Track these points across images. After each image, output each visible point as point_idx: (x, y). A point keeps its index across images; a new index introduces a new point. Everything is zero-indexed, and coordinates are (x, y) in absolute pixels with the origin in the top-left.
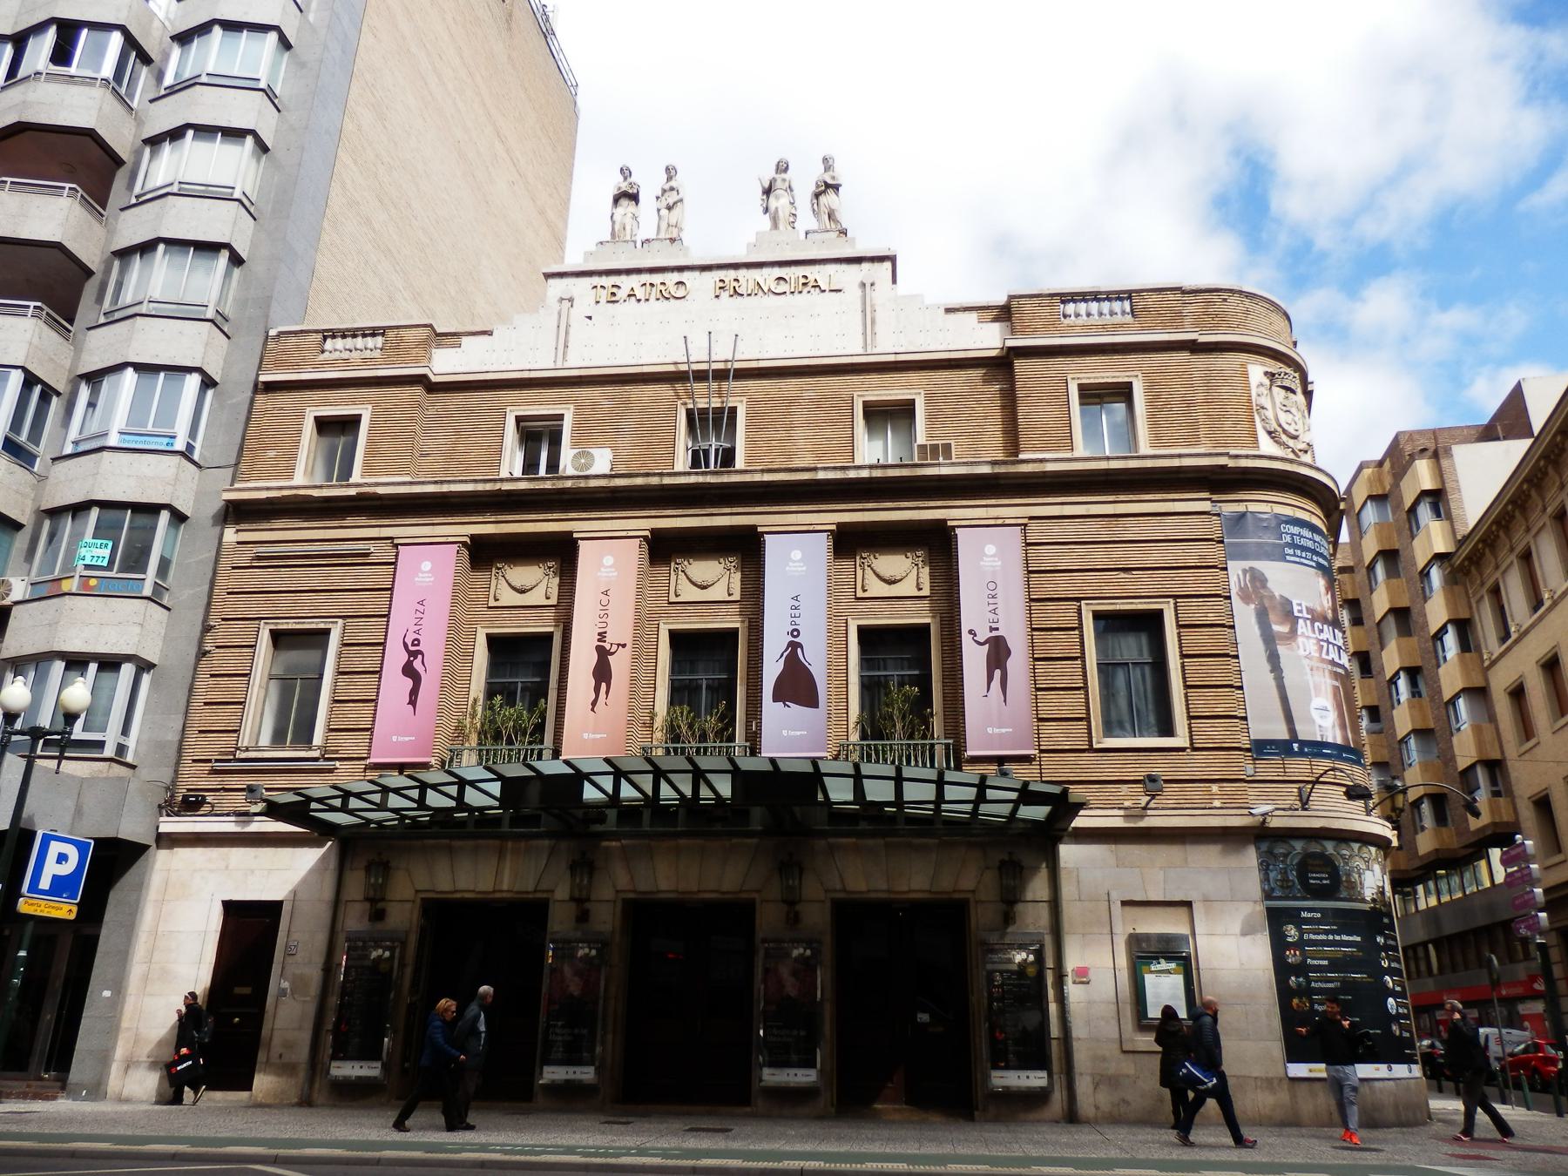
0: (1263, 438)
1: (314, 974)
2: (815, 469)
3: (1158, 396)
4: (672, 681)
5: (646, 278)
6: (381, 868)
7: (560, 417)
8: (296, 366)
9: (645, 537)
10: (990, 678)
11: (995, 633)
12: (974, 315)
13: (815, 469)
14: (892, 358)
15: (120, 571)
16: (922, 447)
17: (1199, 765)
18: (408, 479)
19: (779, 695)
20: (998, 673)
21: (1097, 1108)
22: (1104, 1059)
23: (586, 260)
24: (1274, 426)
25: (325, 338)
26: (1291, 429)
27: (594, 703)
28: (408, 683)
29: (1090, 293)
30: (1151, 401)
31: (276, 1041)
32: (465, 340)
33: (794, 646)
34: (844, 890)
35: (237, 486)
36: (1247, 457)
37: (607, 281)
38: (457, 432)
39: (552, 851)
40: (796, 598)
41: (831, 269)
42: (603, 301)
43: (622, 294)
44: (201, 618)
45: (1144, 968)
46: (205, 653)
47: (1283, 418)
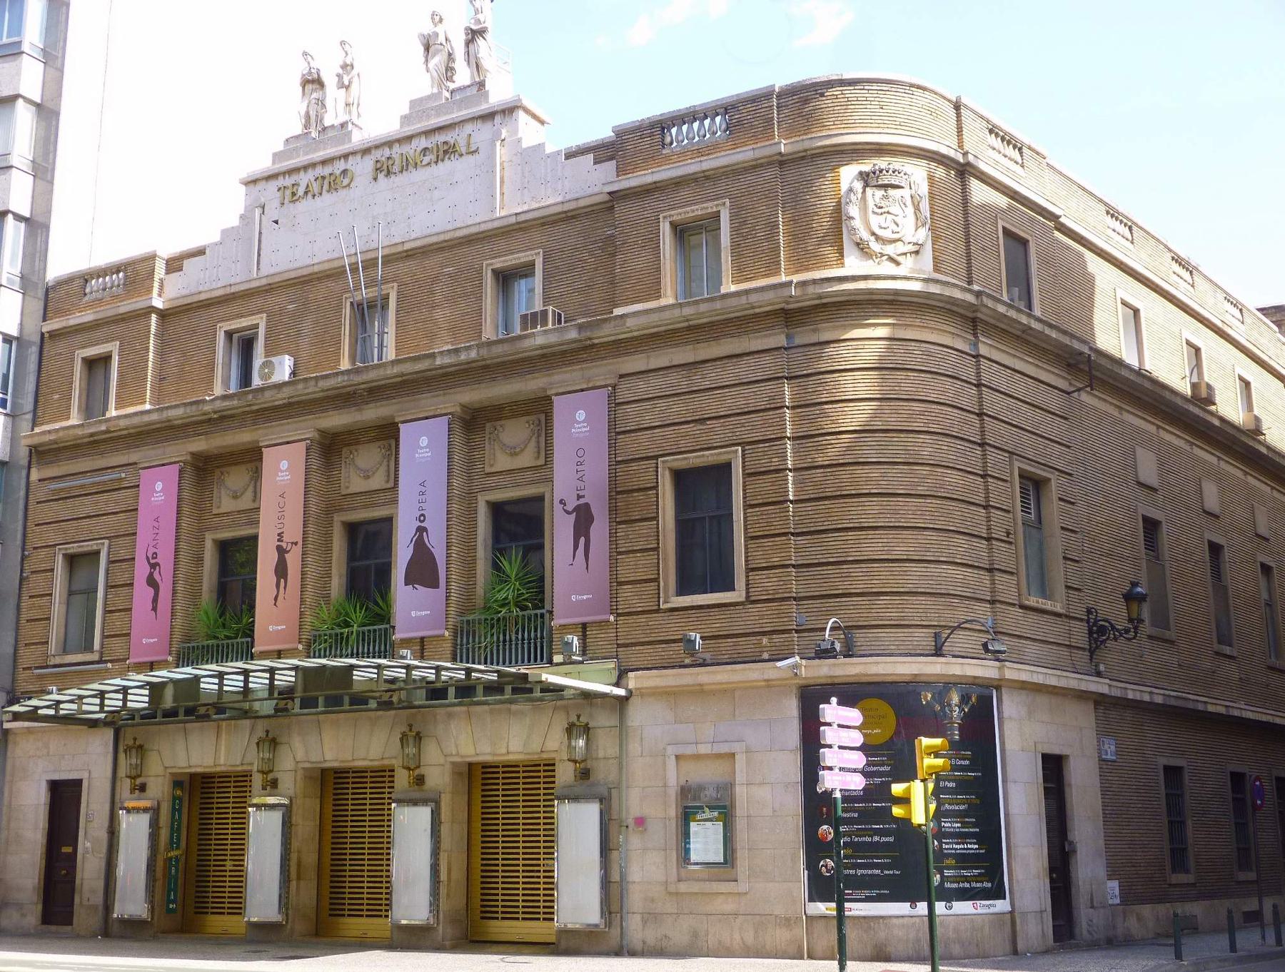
5: (320, 171)
7: (256, 326)
10: (576, 547)
11: (582, 501)
16: (524, 317)
17: (754, 618)
19: (412, 578)
20: (582, 540)
21: (644, 942)
22: (653, 900)
23: (274, 163)
26: (886, 234)
28: (151, 591)
29: (686, 115)
30: (735, 230)
31: (86, 888)
33: (421, 530)
34: (458, 754)
35: (37, 430)
40: (422, 484)
47: (875, 221)
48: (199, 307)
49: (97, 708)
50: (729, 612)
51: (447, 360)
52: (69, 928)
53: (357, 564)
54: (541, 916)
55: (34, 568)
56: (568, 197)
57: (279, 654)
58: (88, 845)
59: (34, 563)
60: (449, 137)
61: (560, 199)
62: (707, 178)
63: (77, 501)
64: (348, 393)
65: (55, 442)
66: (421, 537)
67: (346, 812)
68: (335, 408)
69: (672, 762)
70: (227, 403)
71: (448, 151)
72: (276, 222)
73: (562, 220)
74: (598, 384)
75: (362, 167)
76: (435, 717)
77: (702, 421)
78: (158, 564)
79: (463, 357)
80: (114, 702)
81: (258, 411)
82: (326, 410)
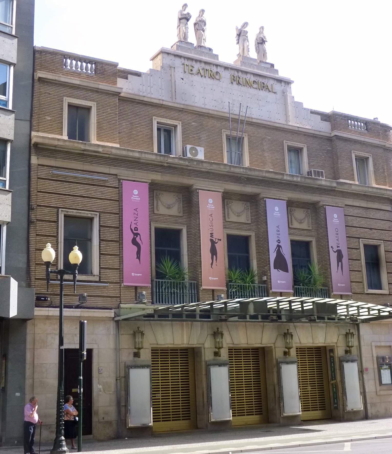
1: (112, 381)
4: (229, 255)
6: (137, 333)
11: (338, 248)
14: (157, 102)
15: (5, 177)
18: (118, 146)
20: (340, 263)
27: (212, 264)
28: (135, 248)
32: (129, 76)
33: (279, 246)
38: (132, 124)
39: (202, 328)
40: (278, 227)
43: (195, 71)
45: (381, 368)
48: (138, 103)
49: (367, 313)
50: (385, 297)
51: (289, 178)
52: (91, 436)
53: (161, 248)
54: (171, 419)
55: (39, 217)
56: (313, 129)
57: (281, 294)
58: (101, 387)
59: (37, 214)
60: (265, 81)
61: (310, 128)
62: (364, 144)
63: (72, 185)
64: (237, 177)
65: (55, 146)
66: (279, 250)
67: (257, 369)
68: (231, 181)
69: (374, 348)
70: (182, 162)
71: (264, 87)
72: (183, 79)
73: (195, 114)
74: (339, 206)
75: (226, 75)
76: (34, 324)
77: (371, 229)
78: (139, 234)
79: (295, 179)
80: (353, 311)
81: (190, 170)
82: (227, 181)
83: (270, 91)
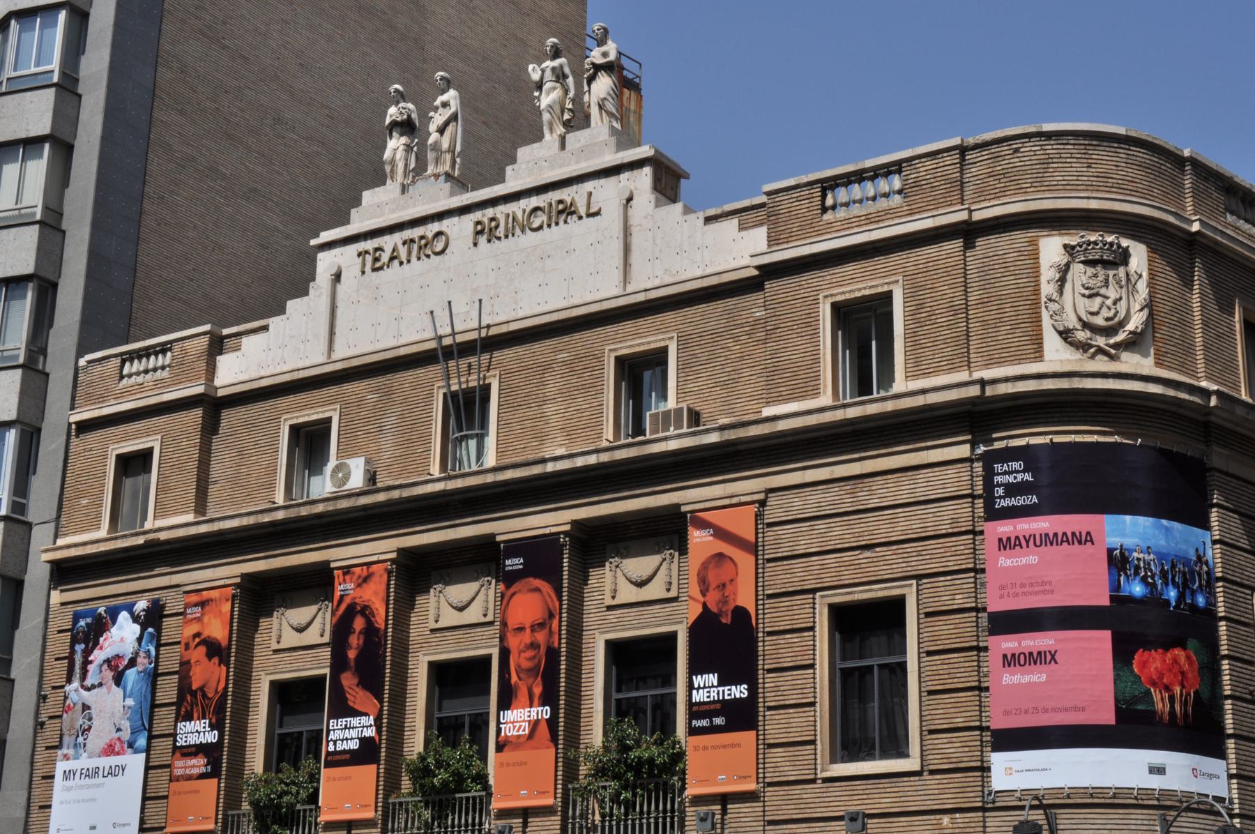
0: (1052, 342)
2: (544, 461)
3: (920, 306)
8: (102, 399)
9: (392, 561)
12: (734, 222)
13: (544, 461)
24: (1072, 322)
25: (123, 362)
30: (913, 315)
35: (60, 542)
36: (1007, 380)
37: (369, 245)
41: (589, 186)
42: (368, 268)
44: (35, 687)
46: (42, 724)
83: (580, 218)
